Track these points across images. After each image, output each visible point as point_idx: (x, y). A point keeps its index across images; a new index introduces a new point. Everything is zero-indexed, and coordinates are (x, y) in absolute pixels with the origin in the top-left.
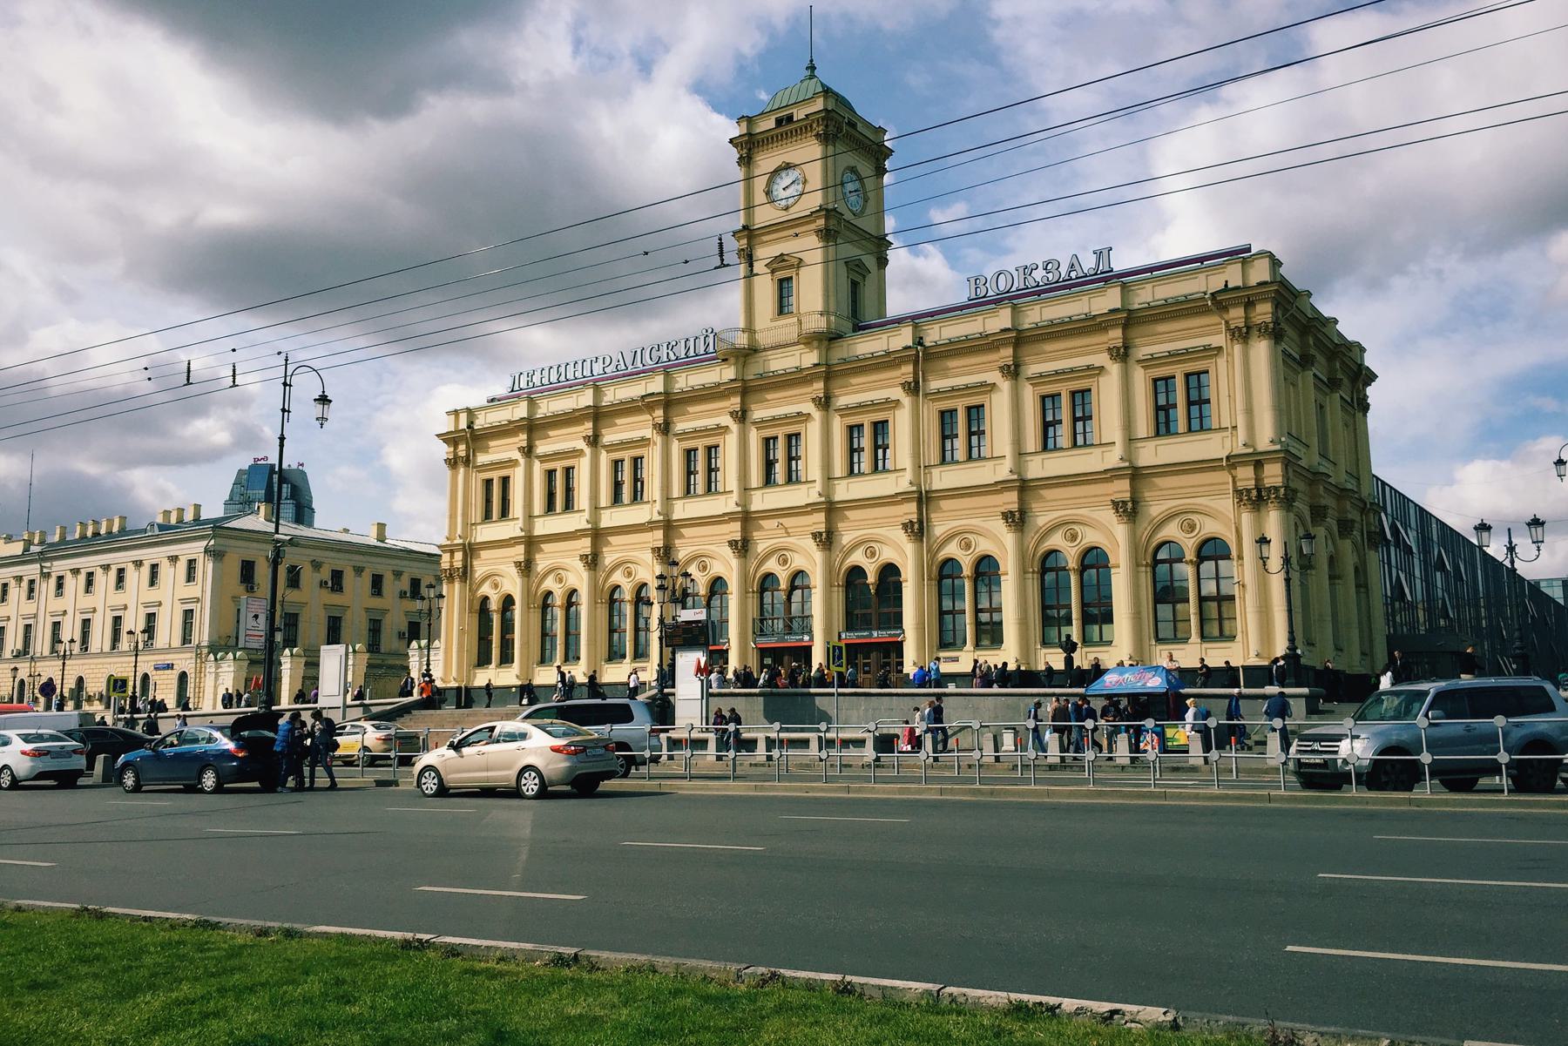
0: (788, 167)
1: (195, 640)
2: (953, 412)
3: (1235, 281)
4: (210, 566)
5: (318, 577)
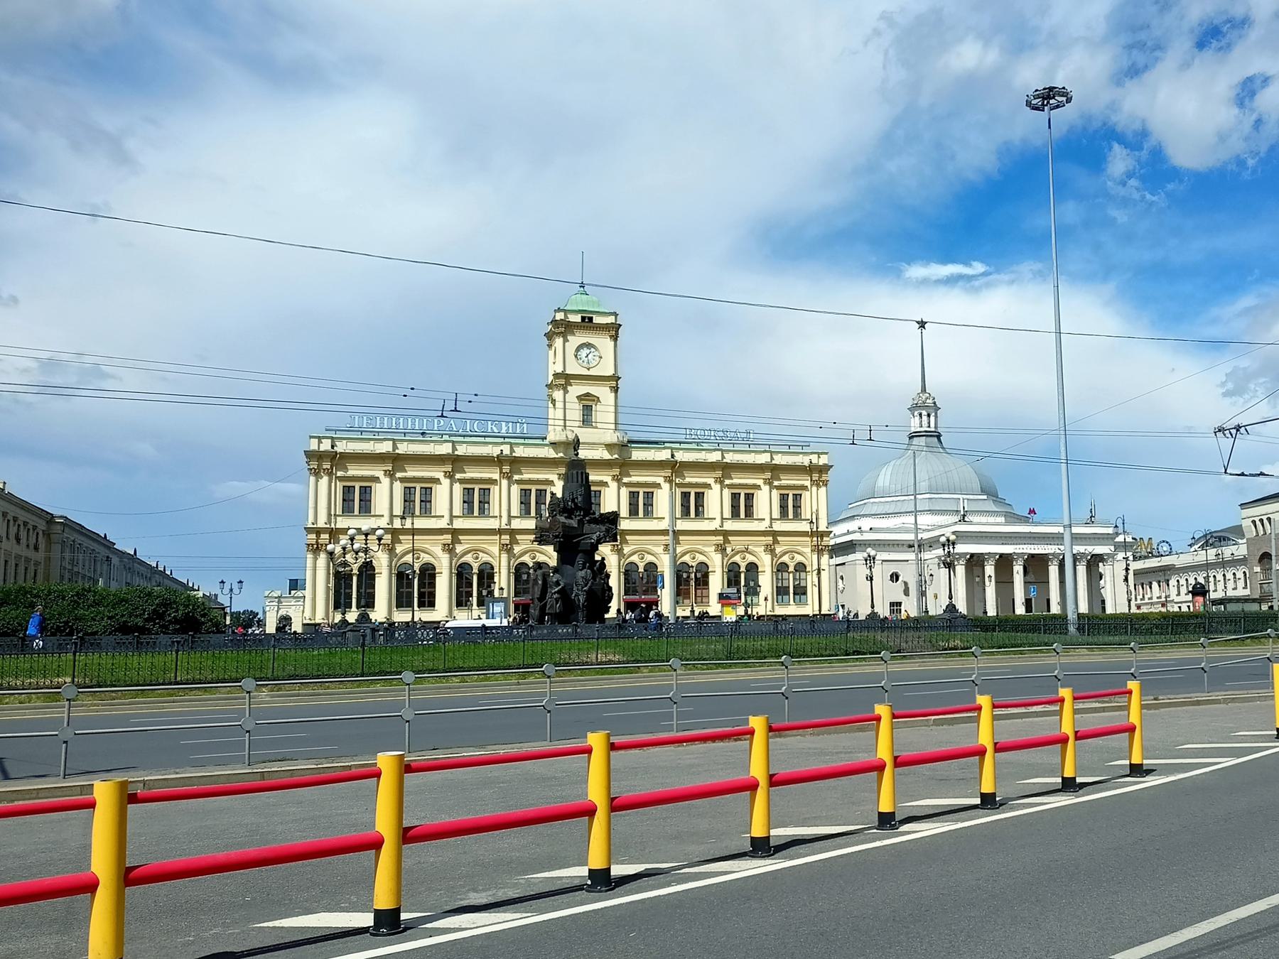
0: (589, 345)
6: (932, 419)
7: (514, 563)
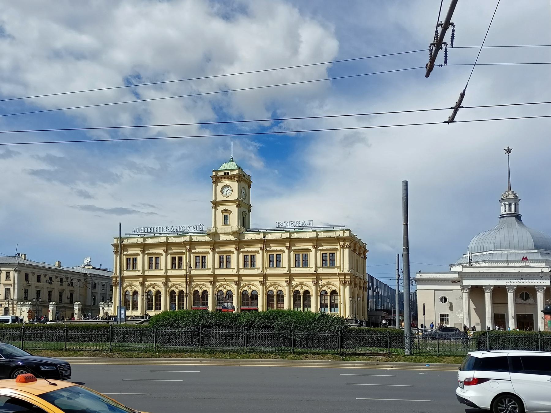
0: (227, 186)
1: (11, 297)
2: (273, 255)
3: (342, 235)
4: (16, 275)
5: (45, 279)
6: (513, 206)
7: (192, 291)
